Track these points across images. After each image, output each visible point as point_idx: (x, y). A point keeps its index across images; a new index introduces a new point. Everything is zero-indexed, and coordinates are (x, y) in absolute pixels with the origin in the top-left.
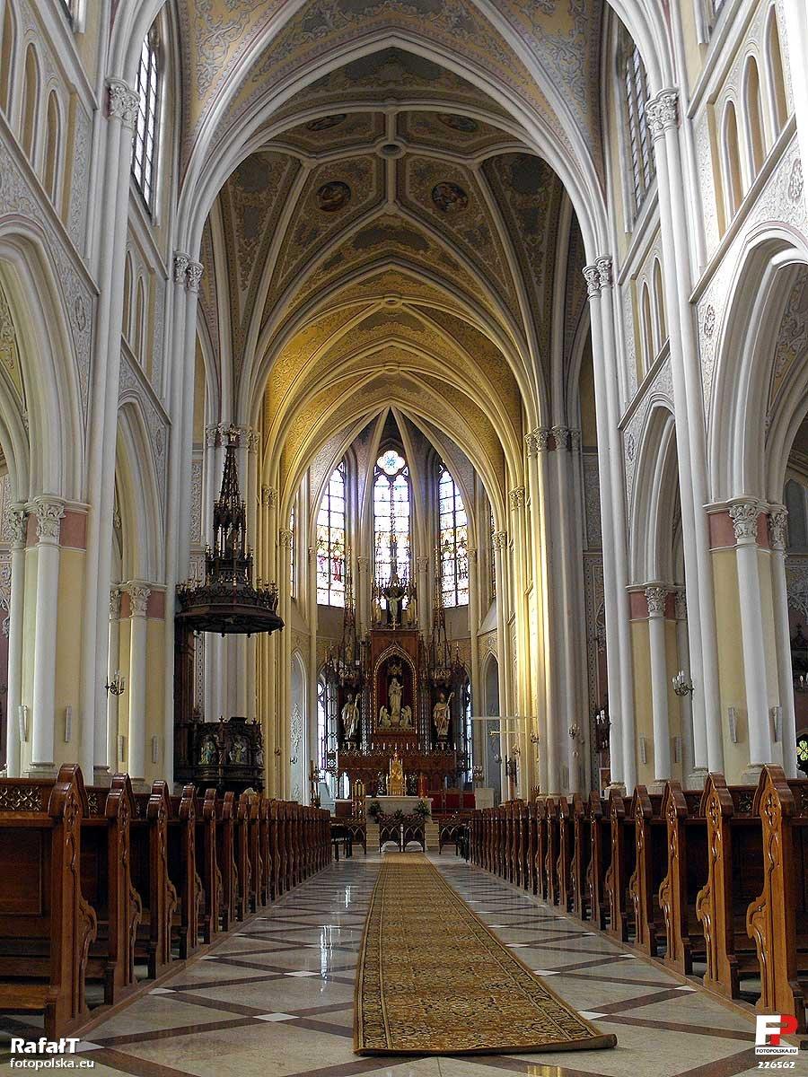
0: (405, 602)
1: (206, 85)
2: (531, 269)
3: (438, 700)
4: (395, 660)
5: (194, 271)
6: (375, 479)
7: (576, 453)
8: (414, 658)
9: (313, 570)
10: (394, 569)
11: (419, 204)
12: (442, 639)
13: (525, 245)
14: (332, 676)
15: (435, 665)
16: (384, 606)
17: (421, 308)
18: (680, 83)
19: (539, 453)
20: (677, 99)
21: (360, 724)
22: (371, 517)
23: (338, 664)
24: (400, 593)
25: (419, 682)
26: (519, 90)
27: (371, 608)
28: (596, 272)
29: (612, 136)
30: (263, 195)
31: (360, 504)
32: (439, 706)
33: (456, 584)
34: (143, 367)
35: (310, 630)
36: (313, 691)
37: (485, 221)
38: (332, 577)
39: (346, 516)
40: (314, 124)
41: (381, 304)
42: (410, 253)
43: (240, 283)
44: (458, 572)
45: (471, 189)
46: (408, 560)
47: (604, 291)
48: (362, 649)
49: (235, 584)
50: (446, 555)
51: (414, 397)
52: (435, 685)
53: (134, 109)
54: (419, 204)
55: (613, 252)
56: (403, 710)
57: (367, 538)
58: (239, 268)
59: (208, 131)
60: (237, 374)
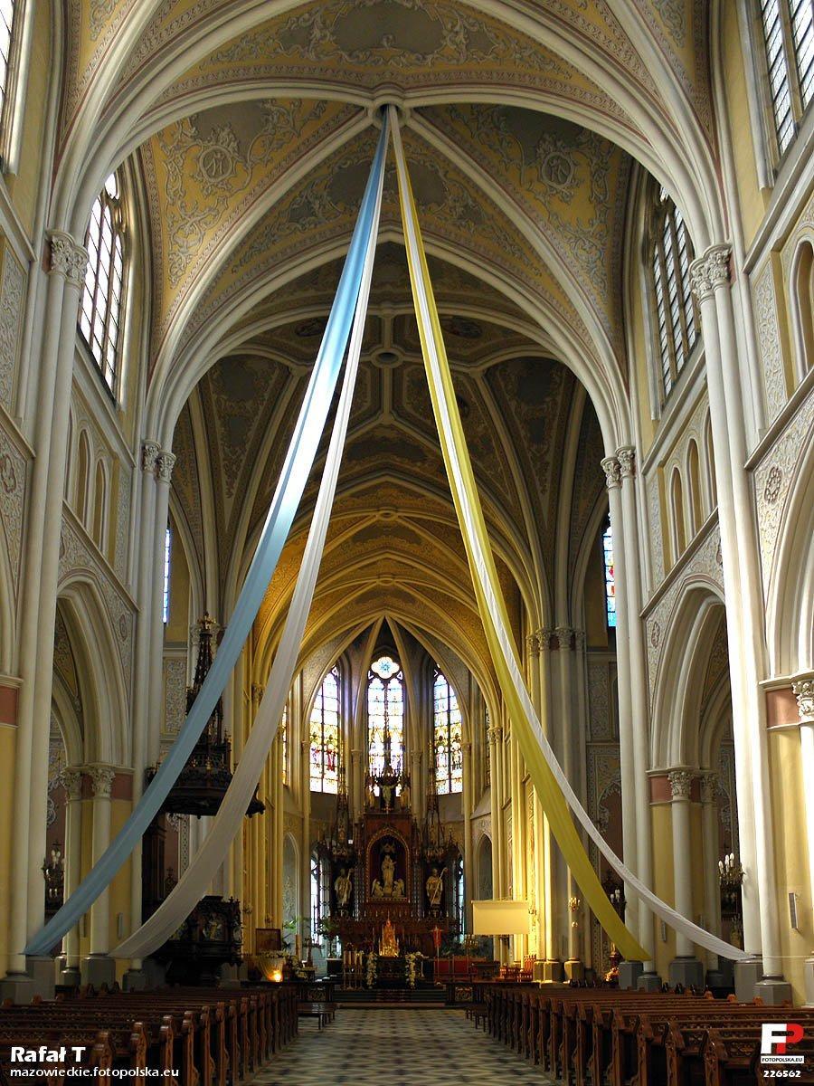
0: (398, 789)
1: (180, 273)
2: (537, 478)
3: (431, 874)
4: (389, 840)
5: (165, 461)
6: (370, 681)
7: (579, 652)
8: (407, 839)
9: (306, 760)
10: (388, 761)
11: (417, 415)
12: (436, 820)
13: (530, 455)
14: (324, 853)
15: (429, 844)
16: (377, 793)
17: (418, 521)
18: (734, 238)
19: (541, 653)
20: (730, 256)
21: (352, 895)
22: (365, 714)
23: (331, 843)
24: (394, 781)
25: (412, 859)
26: (532, 283)
27: (364, 794)
28: (617, 463)
29: (637, 326)
30: (249, 405)
31: (353, 703)
32: (431, 880)
33: (450, 774)
34: (104, 554)
35: (303, 813)
36: (306, 867)
37: (487, 430)
38: (326, 767)
39: (340, 715)
40: (303, 329)
41: (376, 517)
42: (407, 465)
43: (225, 487)
44: (452, 763)
45: (474, 399)
46: (401, 752)
47: (626, 482)
48: (355, 830)
49: (209, 768)
50: (441, 749)
51: (410, 607)
52: (428, 861)
53: (81, 267)
54: (417, 415)
55: (636, 441)
56: (396, 882)
57: (361, 730)
58: (224, 478)
59: (177, 327)
60: (223, 577)
